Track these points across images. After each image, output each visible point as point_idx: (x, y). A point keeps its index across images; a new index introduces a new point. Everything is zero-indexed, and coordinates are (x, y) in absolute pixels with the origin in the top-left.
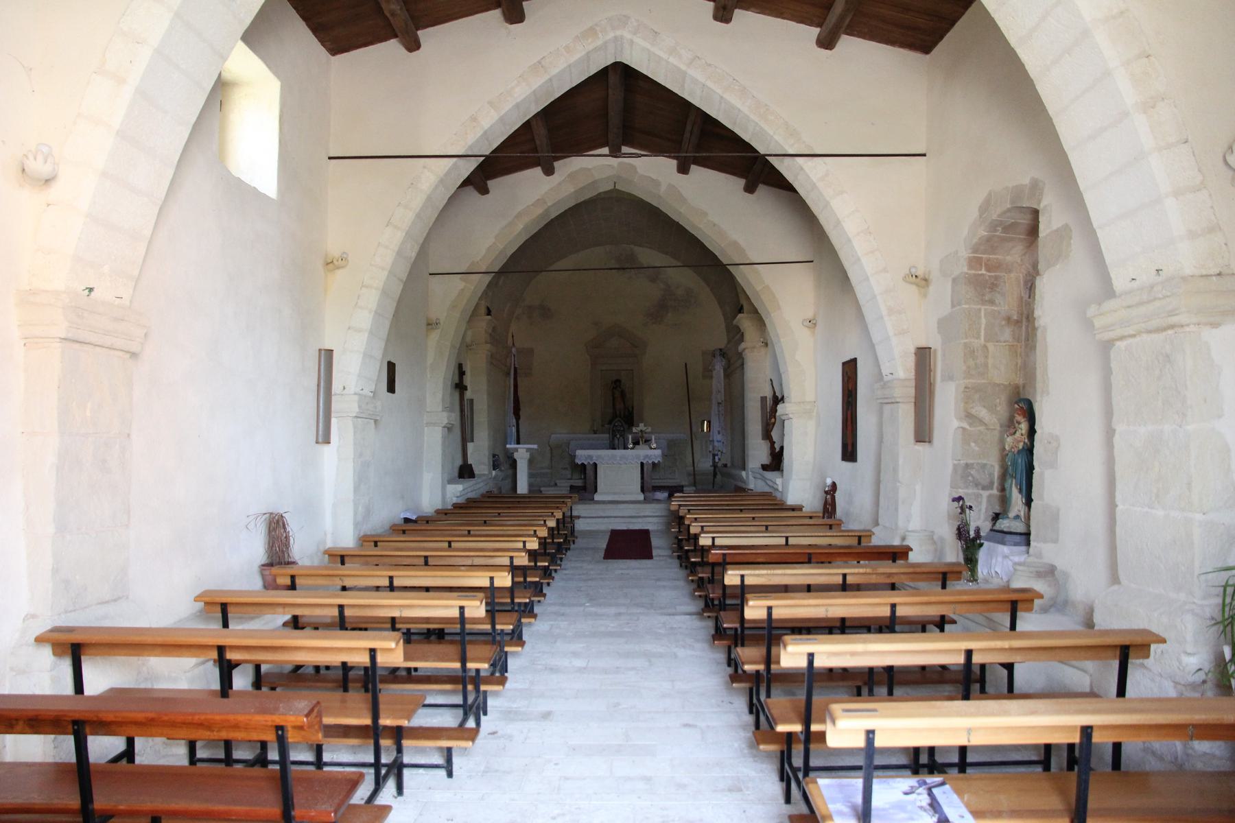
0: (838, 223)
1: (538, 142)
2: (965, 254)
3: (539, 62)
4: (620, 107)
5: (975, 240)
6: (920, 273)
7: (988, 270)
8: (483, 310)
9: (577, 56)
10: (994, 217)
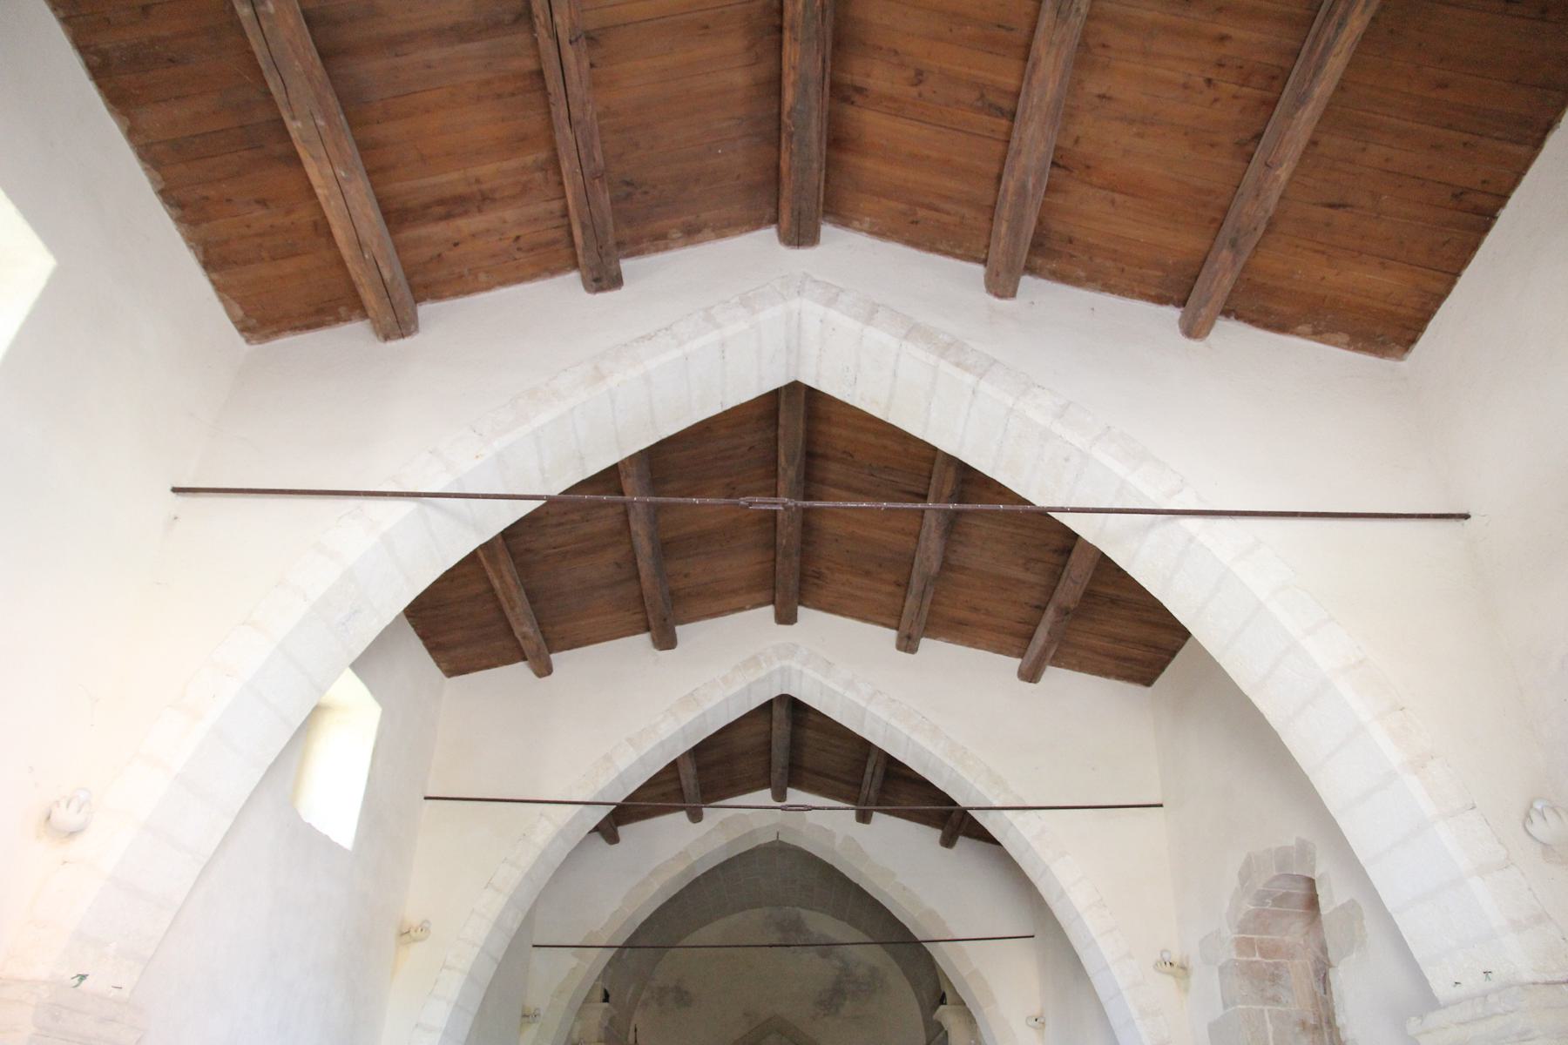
0: (1062, 894)
1: (684, 783)
2: (1229, 934)
3: (691, 694)
4: (786, 745)
5: (1241, 916)
6: (1175, 958)
7: (1264, 956)
8: (599, 995)
9: (736, 688)
10: (1260, 887)
